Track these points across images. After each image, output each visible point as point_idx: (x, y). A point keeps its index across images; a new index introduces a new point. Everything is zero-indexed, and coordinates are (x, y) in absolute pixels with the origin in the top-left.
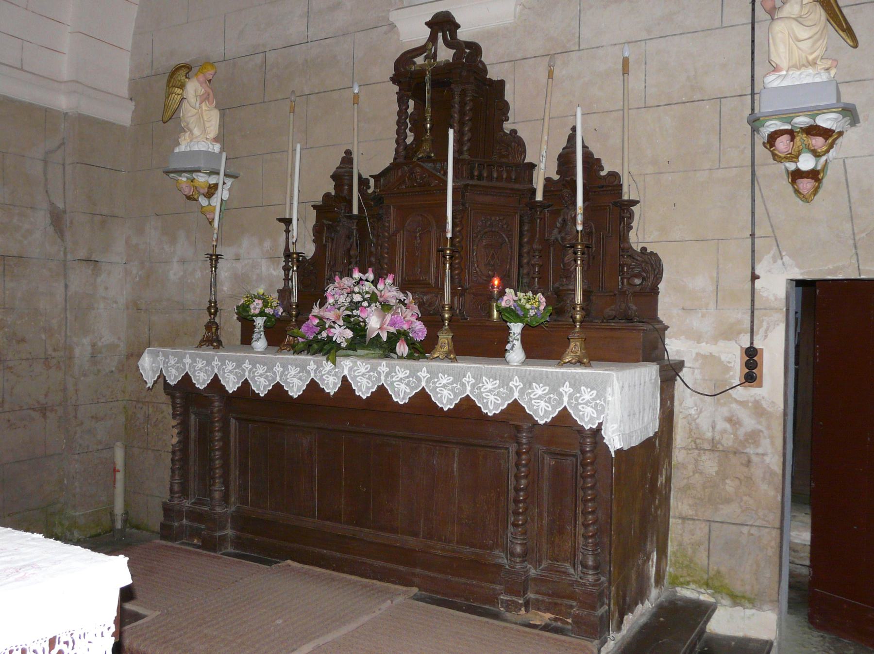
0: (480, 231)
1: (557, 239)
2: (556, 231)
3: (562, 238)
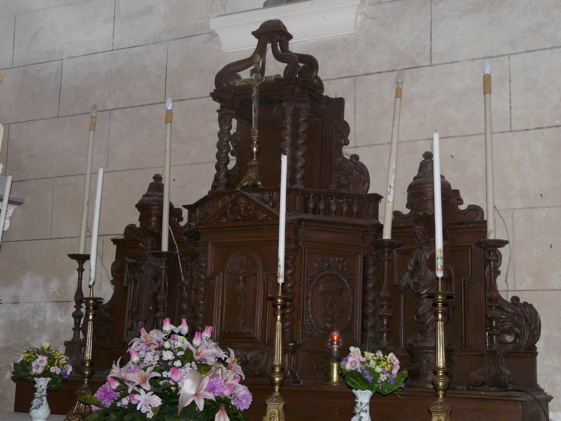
2: (407, 275)
3: (415, 284)
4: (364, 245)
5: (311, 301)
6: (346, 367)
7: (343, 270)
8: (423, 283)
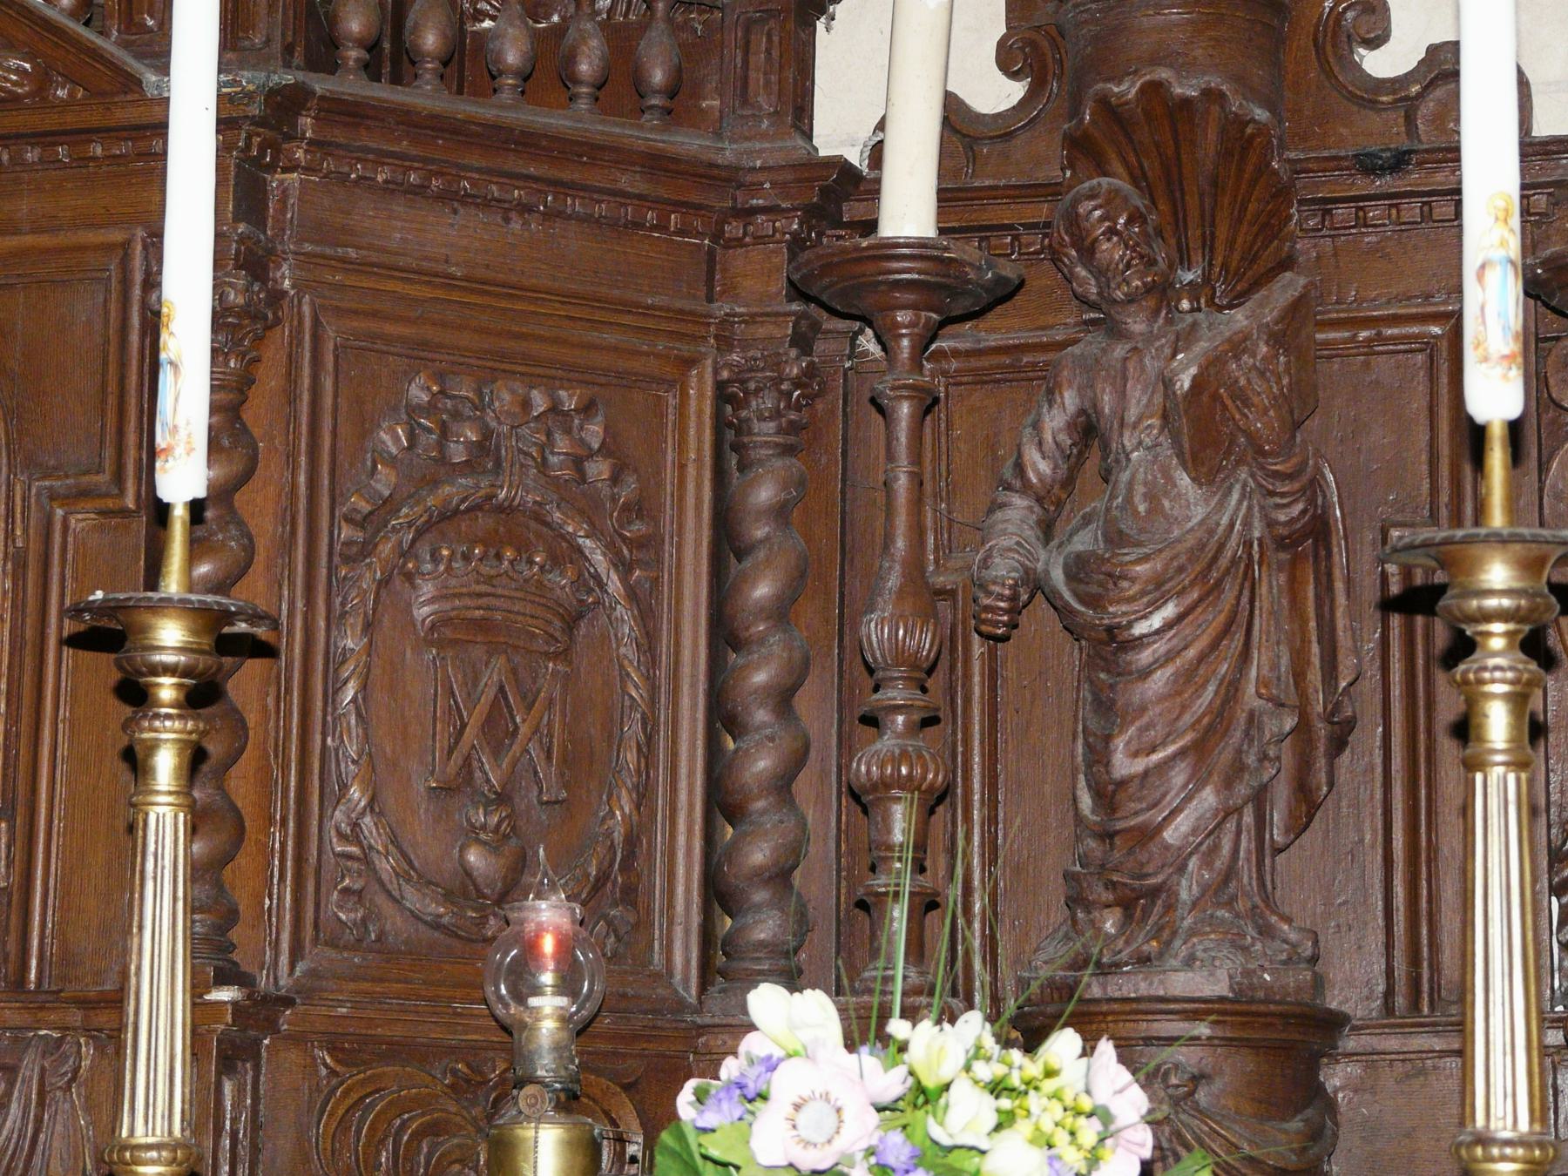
0: (389, 505)
1: (1036, 584)
2: (1018, 512)
3: (1078, 569)
4: (721, 308)
5: (364, 687)
6: (755, 1144)
7: (582, 477)
8: (1145, 558)
